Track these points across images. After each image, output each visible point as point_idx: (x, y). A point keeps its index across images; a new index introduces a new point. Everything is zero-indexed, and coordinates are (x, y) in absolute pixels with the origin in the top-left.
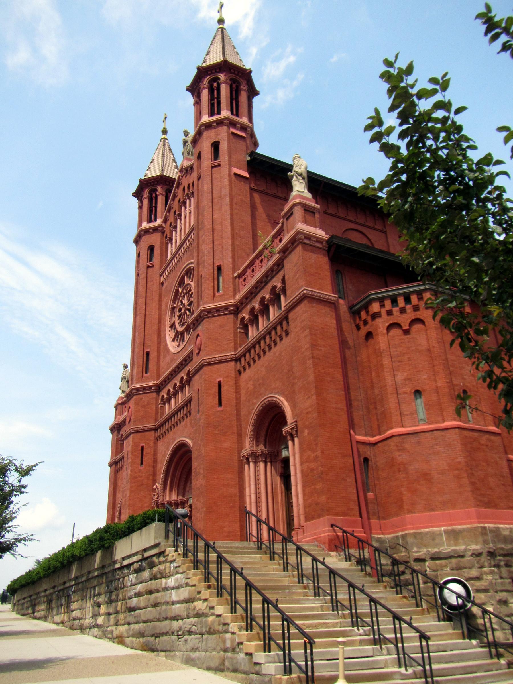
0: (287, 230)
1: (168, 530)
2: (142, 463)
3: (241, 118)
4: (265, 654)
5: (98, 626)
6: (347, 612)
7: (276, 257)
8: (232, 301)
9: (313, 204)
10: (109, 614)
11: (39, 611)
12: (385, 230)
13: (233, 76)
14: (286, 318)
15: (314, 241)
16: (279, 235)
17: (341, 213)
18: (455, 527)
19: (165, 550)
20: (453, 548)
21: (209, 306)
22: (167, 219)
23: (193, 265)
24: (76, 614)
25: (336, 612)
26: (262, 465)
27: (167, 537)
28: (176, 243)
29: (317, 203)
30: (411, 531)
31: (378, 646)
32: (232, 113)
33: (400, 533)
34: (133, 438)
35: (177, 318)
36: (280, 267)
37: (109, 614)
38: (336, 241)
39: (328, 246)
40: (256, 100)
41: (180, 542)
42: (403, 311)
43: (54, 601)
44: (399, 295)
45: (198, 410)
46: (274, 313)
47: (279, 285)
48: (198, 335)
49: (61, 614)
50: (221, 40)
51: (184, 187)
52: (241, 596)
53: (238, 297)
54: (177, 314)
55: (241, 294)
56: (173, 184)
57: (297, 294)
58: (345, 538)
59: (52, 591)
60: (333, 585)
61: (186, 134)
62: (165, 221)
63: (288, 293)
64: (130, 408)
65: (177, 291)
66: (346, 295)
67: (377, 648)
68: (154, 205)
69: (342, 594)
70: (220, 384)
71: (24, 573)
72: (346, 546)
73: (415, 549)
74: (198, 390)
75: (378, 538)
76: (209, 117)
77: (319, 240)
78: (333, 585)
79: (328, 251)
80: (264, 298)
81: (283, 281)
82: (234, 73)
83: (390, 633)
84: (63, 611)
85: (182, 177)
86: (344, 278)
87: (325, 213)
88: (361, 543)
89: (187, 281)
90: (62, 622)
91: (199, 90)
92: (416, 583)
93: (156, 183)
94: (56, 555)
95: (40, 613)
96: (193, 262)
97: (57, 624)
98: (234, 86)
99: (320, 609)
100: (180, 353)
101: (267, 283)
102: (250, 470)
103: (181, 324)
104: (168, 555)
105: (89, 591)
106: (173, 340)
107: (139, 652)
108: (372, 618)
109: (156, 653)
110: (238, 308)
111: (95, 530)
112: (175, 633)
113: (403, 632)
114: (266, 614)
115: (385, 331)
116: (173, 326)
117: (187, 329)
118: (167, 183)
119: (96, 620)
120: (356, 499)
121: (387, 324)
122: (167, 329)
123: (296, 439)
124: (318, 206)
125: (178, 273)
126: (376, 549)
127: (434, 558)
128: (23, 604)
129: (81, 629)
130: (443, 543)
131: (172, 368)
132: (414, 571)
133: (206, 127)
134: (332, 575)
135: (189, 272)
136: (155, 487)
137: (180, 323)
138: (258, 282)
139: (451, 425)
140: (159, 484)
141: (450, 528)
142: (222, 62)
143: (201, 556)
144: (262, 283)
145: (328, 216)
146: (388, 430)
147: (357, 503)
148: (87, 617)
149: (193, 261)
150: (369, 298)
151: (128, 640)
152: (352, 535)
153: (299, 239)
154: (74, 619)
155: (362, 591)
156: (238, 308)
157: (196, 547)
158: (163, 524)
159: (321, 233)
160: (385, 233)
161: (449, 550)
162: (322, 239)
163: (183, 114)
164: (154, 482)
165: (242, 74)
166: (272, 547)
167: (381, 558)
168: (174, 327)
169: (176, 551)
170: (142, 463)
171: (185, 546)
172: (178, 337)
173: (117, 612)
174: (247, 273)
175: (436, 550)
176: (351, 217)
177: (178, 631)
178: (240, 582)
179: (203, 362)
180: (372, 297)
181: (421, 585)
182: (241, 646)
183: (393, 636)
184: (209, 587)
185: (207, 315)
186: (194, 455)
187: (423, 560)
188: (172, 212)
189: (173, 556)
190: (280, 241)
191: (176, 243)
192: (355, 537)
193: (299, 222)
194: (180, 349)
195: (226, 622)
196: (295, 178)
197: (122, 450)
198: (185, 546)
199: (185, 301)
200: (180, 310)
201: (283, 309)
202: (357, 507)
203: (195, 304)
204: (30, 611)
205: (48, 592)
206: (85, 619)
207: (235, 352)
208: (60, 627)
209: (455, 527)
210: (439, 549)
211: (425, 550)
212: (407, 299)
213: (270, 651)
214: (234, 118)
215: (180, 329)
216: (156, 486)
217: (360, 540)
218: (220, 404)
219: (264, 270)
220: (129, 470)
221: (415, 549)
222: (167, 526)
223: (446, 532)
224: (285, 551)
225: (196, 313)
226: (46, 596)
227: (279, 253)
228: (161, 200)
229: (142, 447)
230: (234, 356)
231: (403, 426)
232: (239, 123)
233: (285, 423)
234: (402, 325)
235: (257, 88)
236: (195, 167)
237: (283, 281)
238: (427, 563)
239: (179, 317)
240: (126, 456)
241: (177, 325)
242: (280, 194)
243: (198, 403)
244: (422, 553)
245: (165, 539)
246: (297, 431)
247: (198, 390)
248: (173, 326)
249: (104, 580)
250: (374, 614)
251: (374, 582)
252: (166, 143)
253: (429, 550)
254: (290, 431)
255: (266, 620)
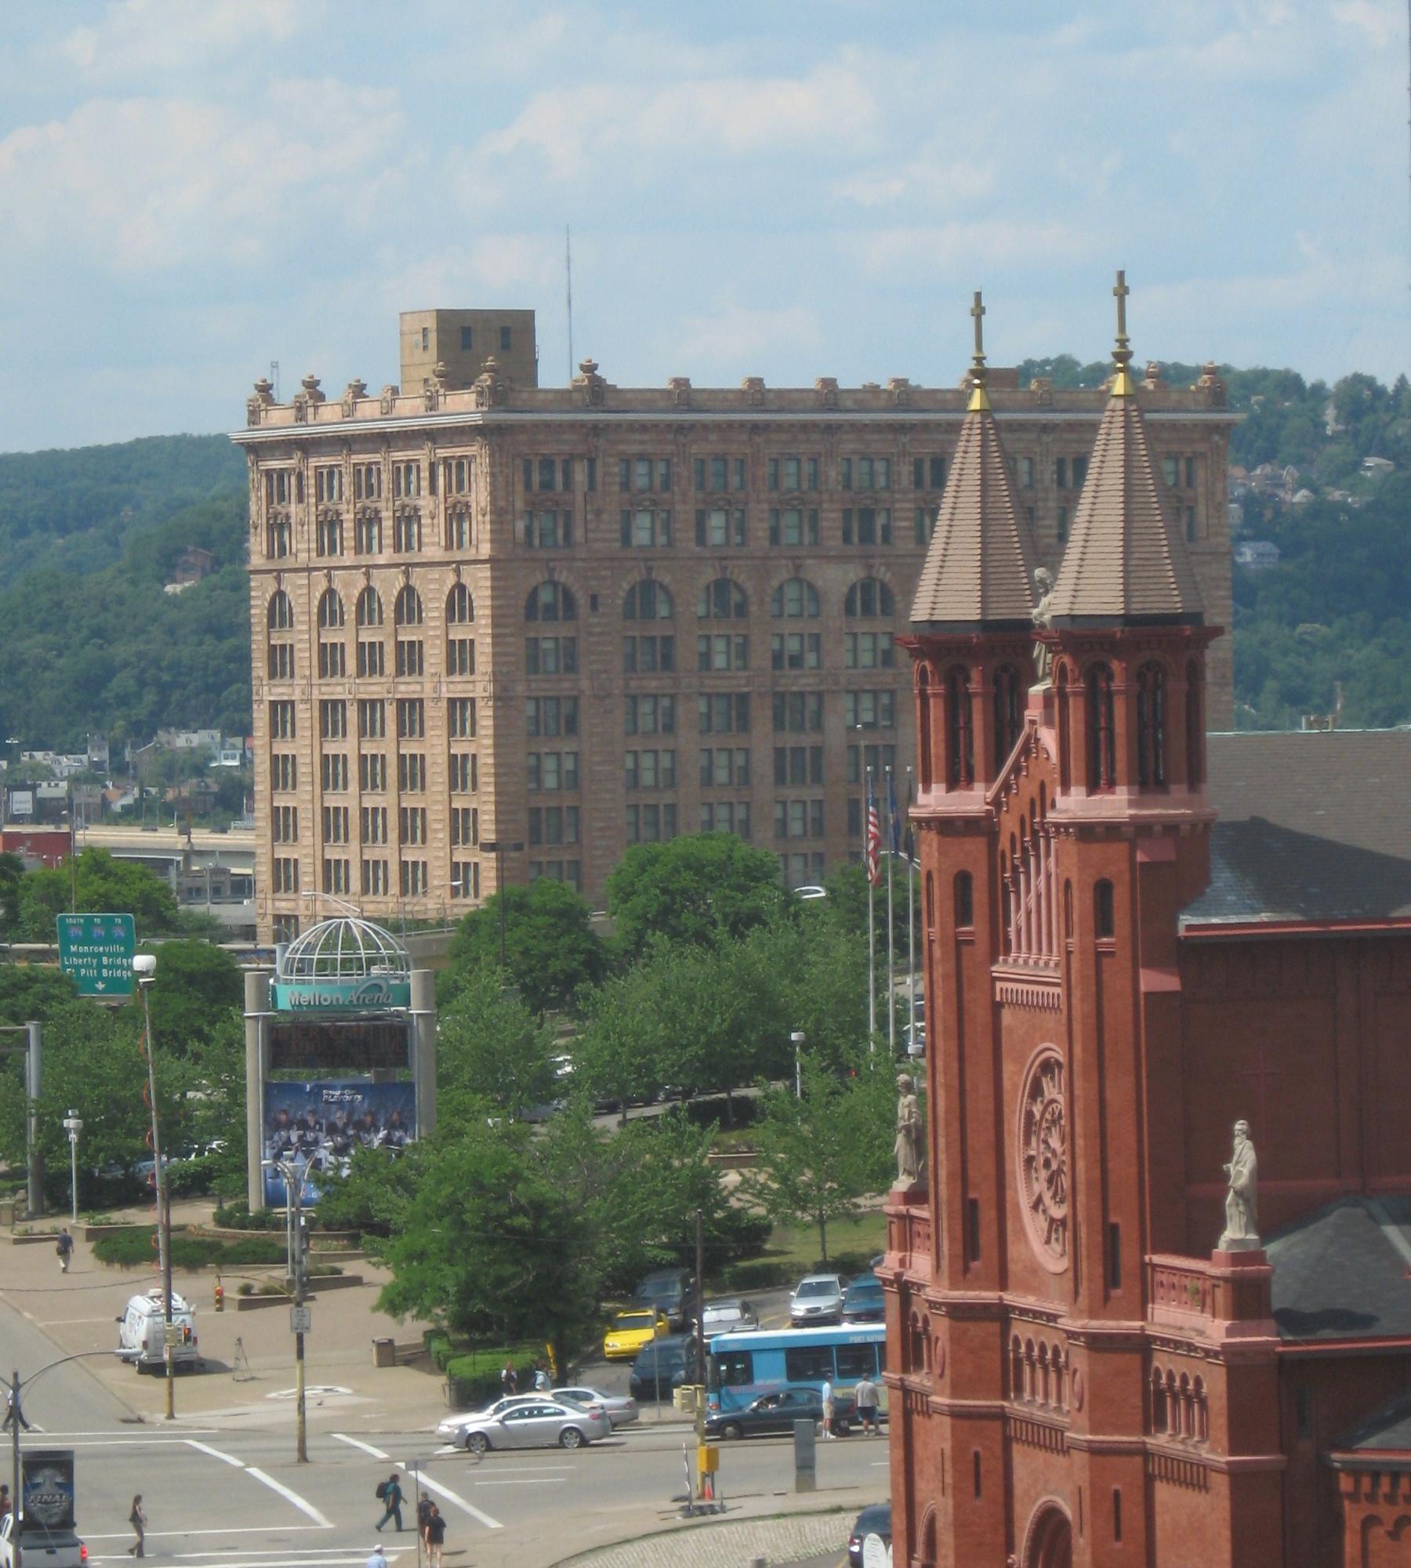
2: (978, 1492)
35: (1045, 1185)
54: (1044, 1174)
65: (1030, 1114)
71: (31, 448)
89: (1046, 1083)
94: (52, 458)
106: (1048, 1241)
111: (46, 447)
137: (1054, 1197)
168: (1041, 1208)
170: (978, 1492)
172: (1057, 1230)
193: (1077, 784)
200: (1047, 1164)
229: (977, 1455)
239: (1050, 1181)
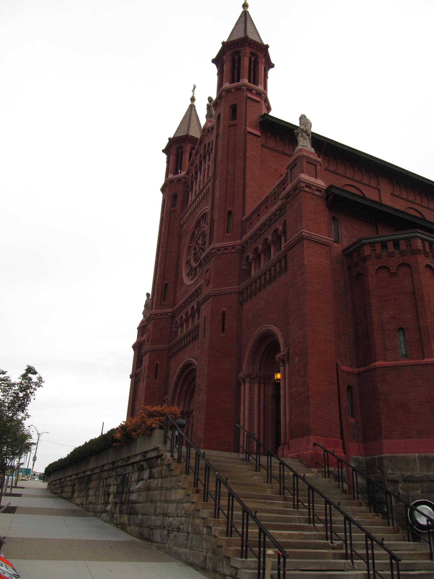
0: (291, 179)
1: (167, 437)
2: (156, 378)
3: (258, 86)
4: (241, 559)
5: (106, 511)
6: (322, 525)
7: (279, 203)
8: (239, 241)
9: (315, 157)
10: (116, 503)
11: (65, 492)
12: (378, 187)
13: (253, 50)
14: (285, 257)
15: (314, 190)
16: (283, 185)
17: (341, 170)
18: (428, 454)
19: (163, 454)
20: (425, 473)
21: (218, 245)
22: (189, 172)
23: (208, 210)
24: (91, 499)
25: (312, 525)
26: (256, 386)
27: (165, 443)
28: (196, 192)
29: (319, 157)
30: (387, 455)
31: (349, 561)
32: (249, 81)
33: (377, 456)
34: (150, 355)
36: (283, 212)
37: (116, 503)
38: (334, 191)
39: (326, 195)
40: (271, 72)
41: (176, 448)
42: (391, 255)
43: (77, 486)
44: (390, 241)
45: (204, 335)
46: (274, 255)
47: (281, 228)
48: (208, 270)
49: (81, 497)
50: (244, 21)
51: (206, 144)
52: (224, 502)
53: (245, 238)
55: (247, 236)
56: (197, 143)
57: (296, 236)
58: (326, 456)
59: (75, 477)
60: (311, 498)
61: (210, 100)
62: (188, 173)
63: (288, 234)
64: (148, 330)
66: (340, 240)
67: (348, 562)
68: (179, 160)
69: (320, 506)
70: (224, 314)
72: (326, 464)
73: (390, 471)
74: (205, 317)
75: (356, 458)
76: (230, 84)
77: (319, 189)
78: (311, 498)
79: (327, 199)
80: (267, 239)
81: (285, 224)
82: (253, 48)
83: (362, 549)
84: (82, 496)
85: (204, 136)
86: (339, 225)
87: (326, 169)
88: (340, 463)
90: (82, 504)
91: (223, 62)
92: (389, 502)
93: (182, 141)
95: (66, 494)
96: (207, 208)
97: (78, 505)
98: (253, 59)
99: (298, 521)
100: (193, 285)
101: (270, 226)
102: (246, 388)
103: (196, 260)
104: (165, 459)
105: (102, 481)
107: (137, 540)
108: (345, 533)
109: (150, 543)
110: (243, 248)
112: (167, 528)
113: (374, 548)
114: (245, 521)
115: (374, 273)
116: (188, 262)
117: (200, 265)
118: (192, 142)
119: (129, 496)
120: (339, 422)
121: (376, 267)
122: (184, 265)
123: (287, 365)
124: (319, 160)
125: (197, 217)
126: (354, 470)
127: (406, 480)
128: (55, 485)
129: (94, 512)
130: (417, 468)
131: (185, 298)
132: (388, 492)
133: (226, 92)
134: (311, 491)
135: (204, 216)
136: (165, 398)
138: (262, 225)
139: (430, 361)
140: (169, 396)
141: (423, 455)
142: (243, 38)
143: (192, 462)
144: (265, 226)
145: (329, 173)
146: (371, 363)
147: (339, 426)
148: (100, 503)
149: (208, 207)
150: (361, 243)
151: (129, 528)
152: (333, 455)
153: (301, 187)
154: (90, 503)
155: (338, 508)
156: (243, 248)
157: (188, 453)
158: (162, 432)
159: (321, 183)
160: (379, 190)
161: (422, 475)
162: (321, 188)
163: (208, 85)
164: (166, 394)
165: (261, 48)
166: (258, 459)
167: (358, 476)
169: (172, 456)
171: (180, 452)
172: (192, 272)
173: (122, 503)
174: (254, 218)
175: (409, 474)
176: (349, 174)
177: (168, 527)
178: (224, 490)
179: (211, 293)
180: (364, 241)
181: (394, 504)
182: (220, 549)
183: (364, 552)
184: (197, 491)
185: (216, 253)
186: (198, 374)
187: (397, 482)
188: (194, 166)
189: (169, 460)
190: (284, 188)
191: (196, 192)
192: (336, 457)
194: (193, 282)
195: (210, 525)
196: (300, 135)
197: (141, 366)
198: (180, 452)
199: (200, 242)
200: (195, 249)
201: (283, 249)
202: (339, 430)
203: (207, 243)
204: (59, 491)
205: (72, 478)
206: (98, 504)
207: (239, 286)
208: (79, 508)
209: (428, 454)
210: (412, 473)
211: (399, 473)
212: (396, 244)
213: (246, 558)
214: (251, 85)
215: (194, 265)
216: (167, 398)
217: (339, 460)
218: (223, 331)
219: (268, 215)
220: (145, 382)
221: (390, 471)
222: (166, 433)
223: (419, 458)
224: (269, 464)
225: (207, 251)
226: (71, 480)
227: (282, 199)
228: (186, 156)
230: (238, 290)
231: (385, 360)
232: (255, 90)
233: (279, 351)
234: (390, 268)
235: (273, 61)
236: (215, 128)
237: (285, 224)
238: (400, 485)
239: (194, 254)
240: (143, 370)
241: (192, 261)
242: (287, 152)
243: (204, 328)
244: (396, 475)
245: (164, 444)
246: (288, 358)
247: (205, 317)
248: (188, 262)
249: (114, 474)
250: (348, 530)
251: (350, 499)
252: (193, 109)
253: (403, 473)
254: (283, 357)
255: (245, 527)
